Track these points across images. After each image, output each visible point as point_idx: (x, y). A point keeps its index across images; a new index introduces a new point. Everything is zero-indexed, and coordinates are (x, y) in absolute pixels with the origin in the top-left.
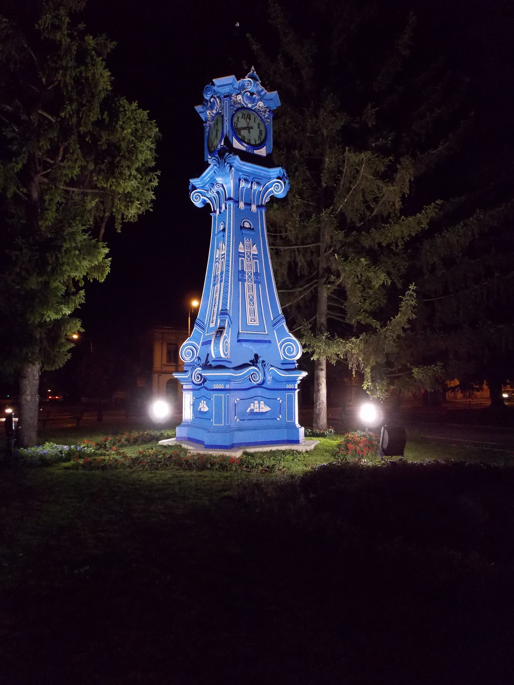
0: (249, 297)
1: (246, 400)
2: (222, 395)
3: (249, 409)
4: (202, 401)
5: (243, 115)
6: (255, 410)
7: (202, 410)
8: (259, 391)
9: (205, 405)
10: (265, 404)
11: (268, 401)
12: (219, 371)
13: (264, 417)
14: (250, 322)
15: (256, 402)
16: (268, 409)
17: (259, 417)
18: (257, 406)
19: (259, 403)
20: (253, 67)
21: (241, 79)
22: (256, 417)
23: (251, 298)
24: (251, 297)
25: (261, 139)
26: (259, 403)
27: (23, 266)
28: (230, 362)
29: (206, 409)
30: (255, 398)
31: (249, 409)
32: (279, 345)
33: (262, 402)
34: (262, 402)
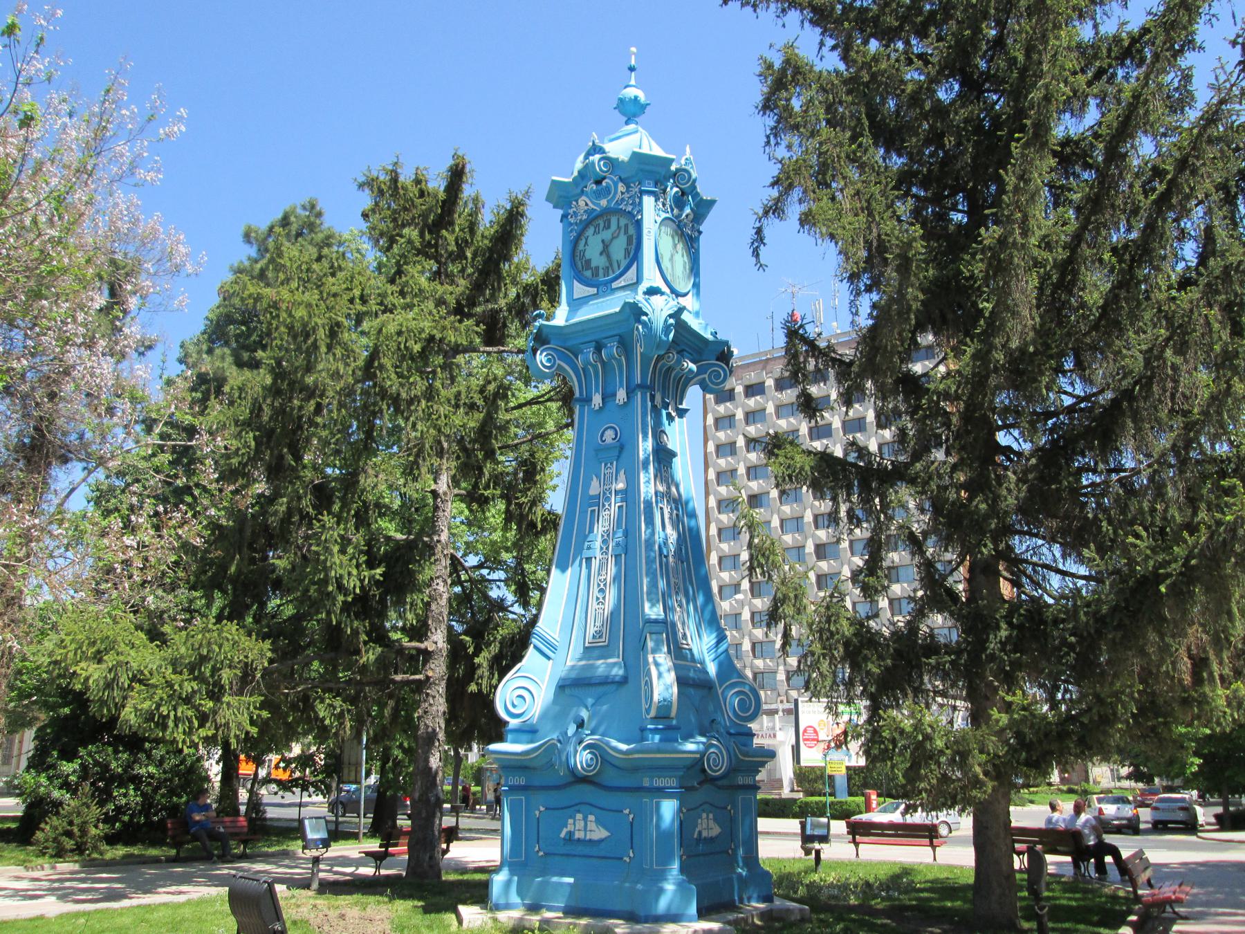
3: (565, 831)
4: (704, 815)
6: (578, 835)
7: (705, 834)
8: (586, 792)
10: (598, 822)
11: (605, 815)
12: (1226, 849)
13: (594, 851)
15: (579, 816)
17: (586, 850)
18: (580, 825)
19: (585, 819)
22: (580, 849)
26: (585, 819)
29: (716, 830)
31: (565, 831)
33: (591, 818)
34: (591, 818)
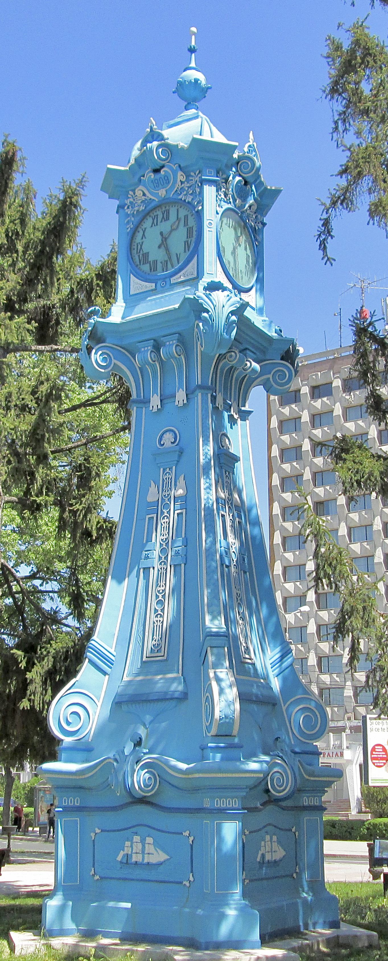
0: (157, 597)
1: (112, 834)
3: (122, 853)
4: (268, 837)
5: (153, 220)
9: (275, 845)
10: (156, 844)
15: (137, 838)
16: (161, 857)
19: (143, 841)
22: (139, 873)
23: (160, 598)
24: (160, 596)
25: (189, 247)
26: (143, 841)
27: (254, 153)
30: (134, 830)
31: (122, 853)
32: (284, 708)
33: (149, 840)
34: (149, 840)
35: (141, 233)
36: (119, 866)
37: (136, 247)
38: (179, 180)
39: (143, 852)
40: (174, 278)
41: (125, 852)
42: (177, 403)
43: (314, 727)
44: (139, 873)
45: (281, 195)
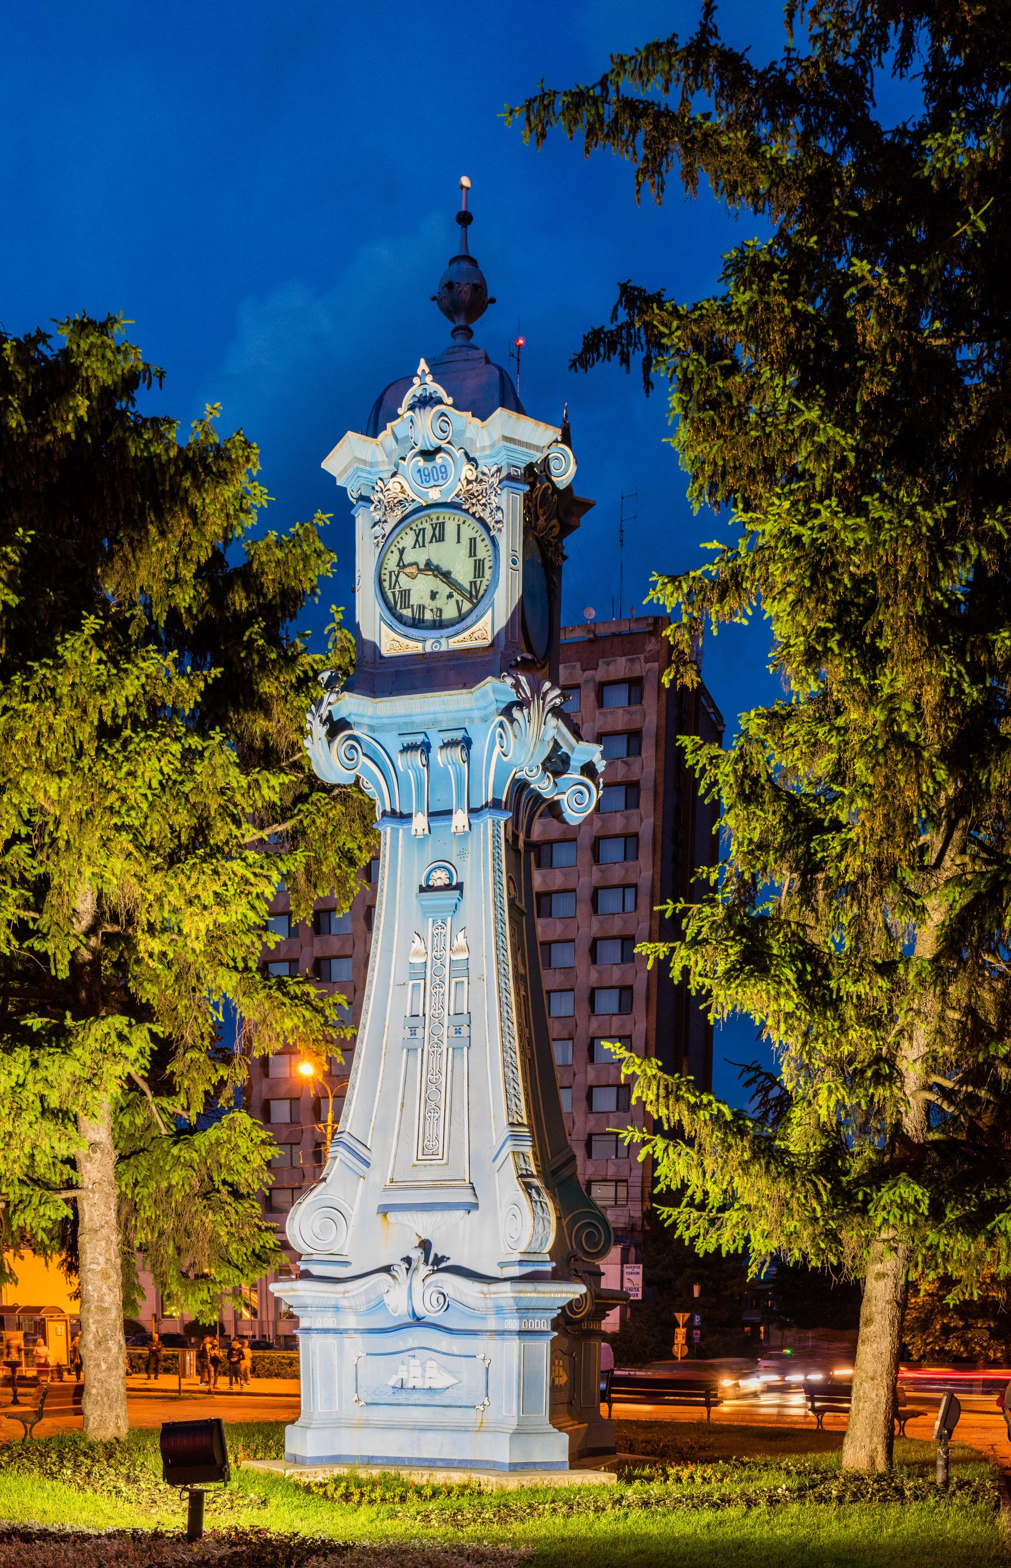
2: (330, 1339)
5: (418, 536)
13: (437, 1400)
14: (420, 1157)
18: (417, 1371)
19: (423, 1365)
20: (422, 361)
21: (389, 425)
22: (416, 1398)
26: (423, 1365)
28: (346, 1263)
30: (411, 1353)
35: (396, 556)
36: (391, 1391)
37: (387, 577)
38: (463, 478)
39: (423, 1377)
40: (456, 639)
41: (400, 1377)
42: (453, 830)
43: (596, 1245)
44: (416, 1398)
45: (591, 512)
